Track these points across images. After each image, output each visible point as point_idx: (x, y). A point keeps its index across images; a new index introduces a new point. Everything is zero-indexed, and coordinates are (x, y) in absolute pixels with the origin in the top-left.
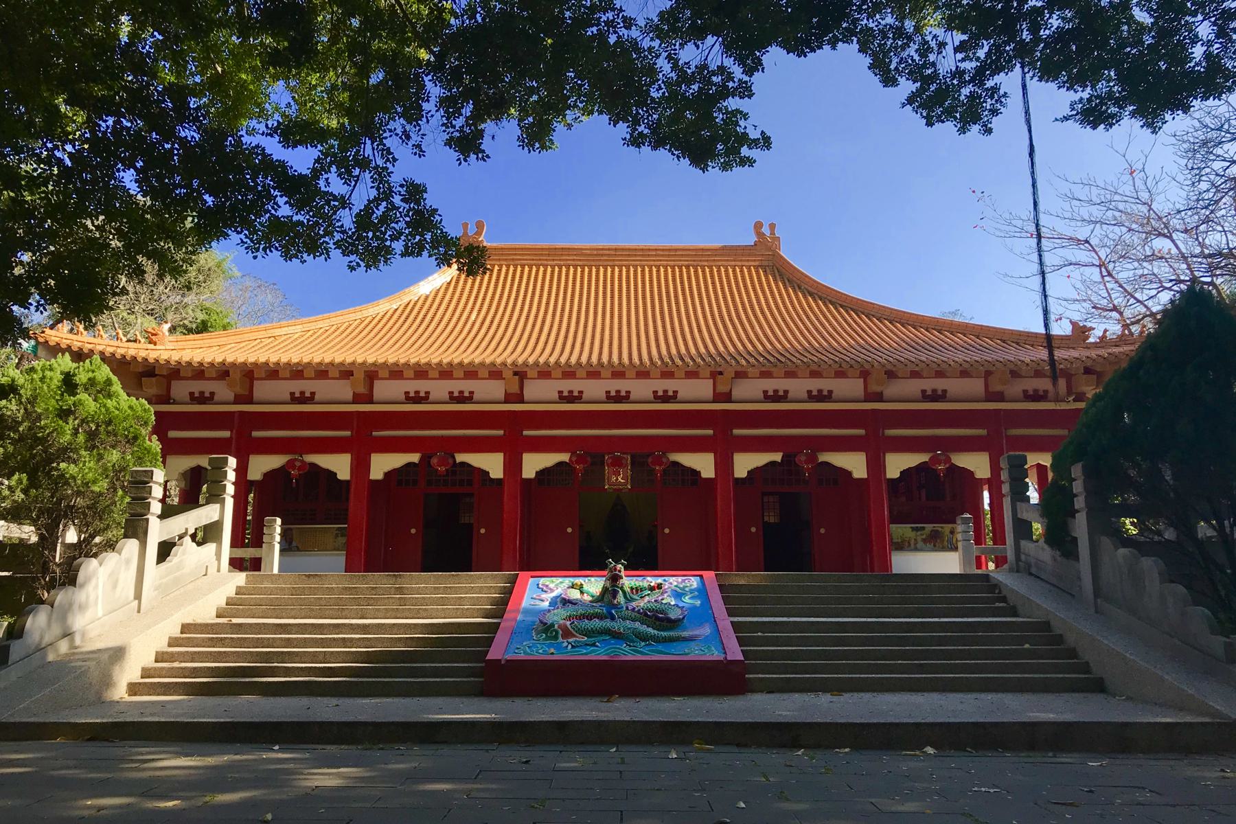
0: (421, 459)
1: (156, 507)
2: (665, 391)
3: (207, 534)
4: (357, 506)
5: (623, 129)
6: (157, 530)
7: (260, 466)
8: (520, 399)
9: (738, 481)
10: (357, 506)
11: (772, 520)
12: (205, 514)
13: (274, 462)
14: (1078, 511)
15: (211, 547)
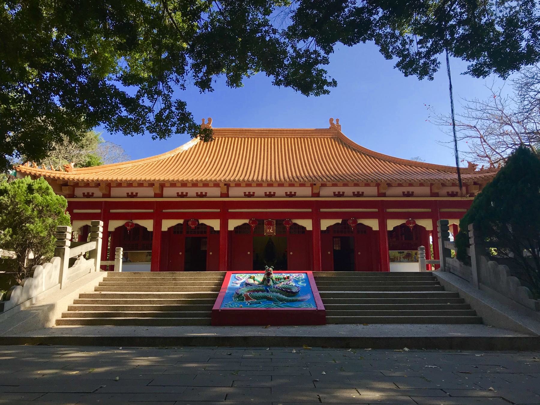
0: (184, 222)
1: (68, 243)
2: (270, 193)
3: (90, 255)
4: (156, 243)
5: (272, 78)
6: (69, 253)
7: (114, 225)
8: (227, 196)
9: (390, 232)
10: (156, 243)
11: (337, 249)
12: (90, 246)
13: (120, 223)
14: (471, 245)
15: (92, 261)
